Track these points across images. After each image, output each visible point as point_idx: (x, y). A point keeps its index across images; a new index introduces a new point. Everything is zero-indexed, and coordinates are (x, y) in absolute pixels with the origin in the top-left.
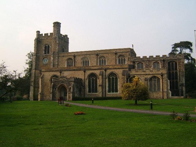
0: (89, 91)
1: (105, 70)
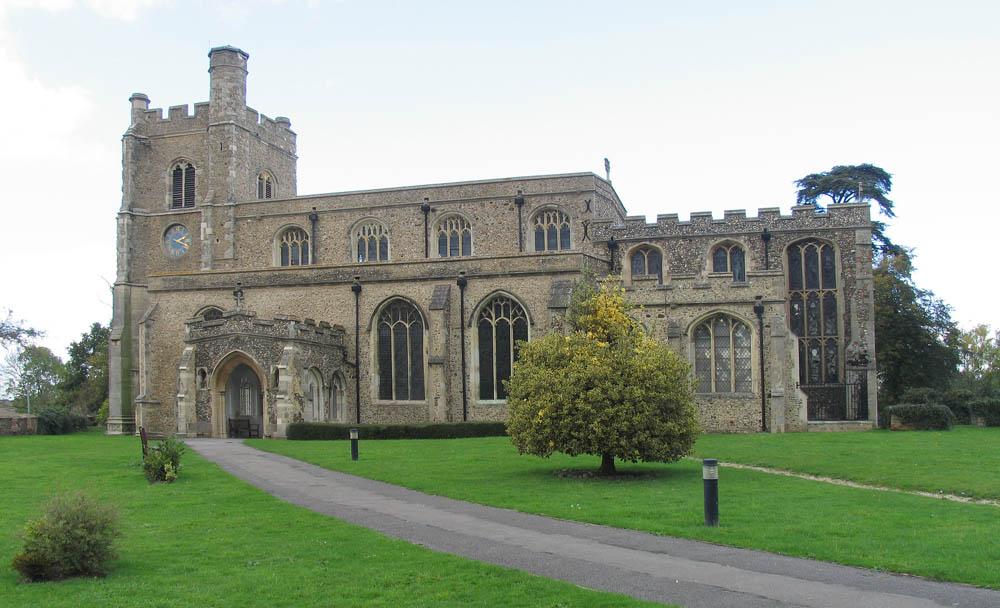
0: (385, 393)
1: (462, 284)
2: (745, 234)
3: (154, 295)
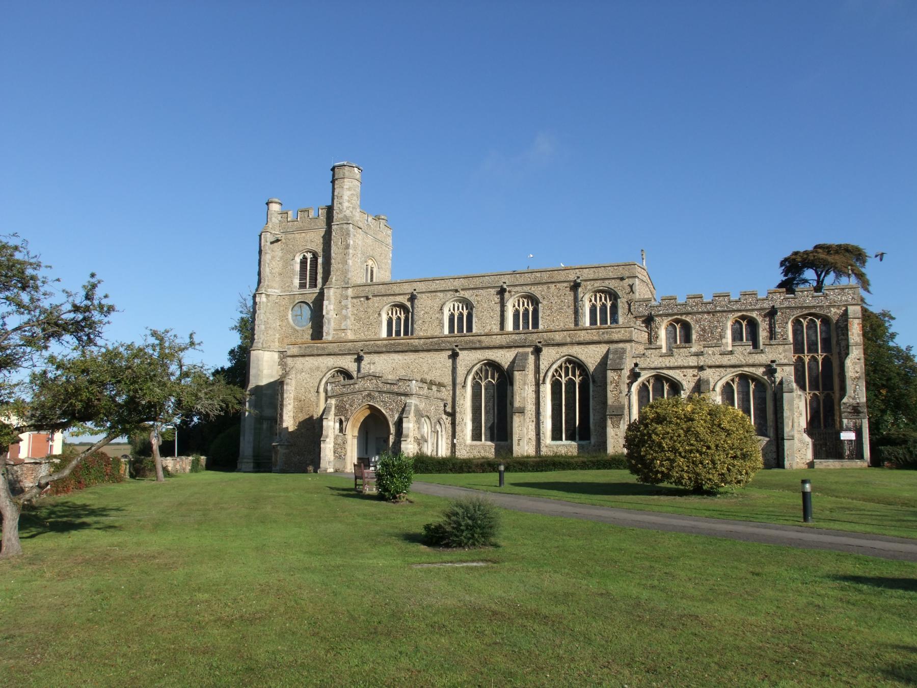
1: (537, 351)
2: (757, 310)
3: (291, 359)
